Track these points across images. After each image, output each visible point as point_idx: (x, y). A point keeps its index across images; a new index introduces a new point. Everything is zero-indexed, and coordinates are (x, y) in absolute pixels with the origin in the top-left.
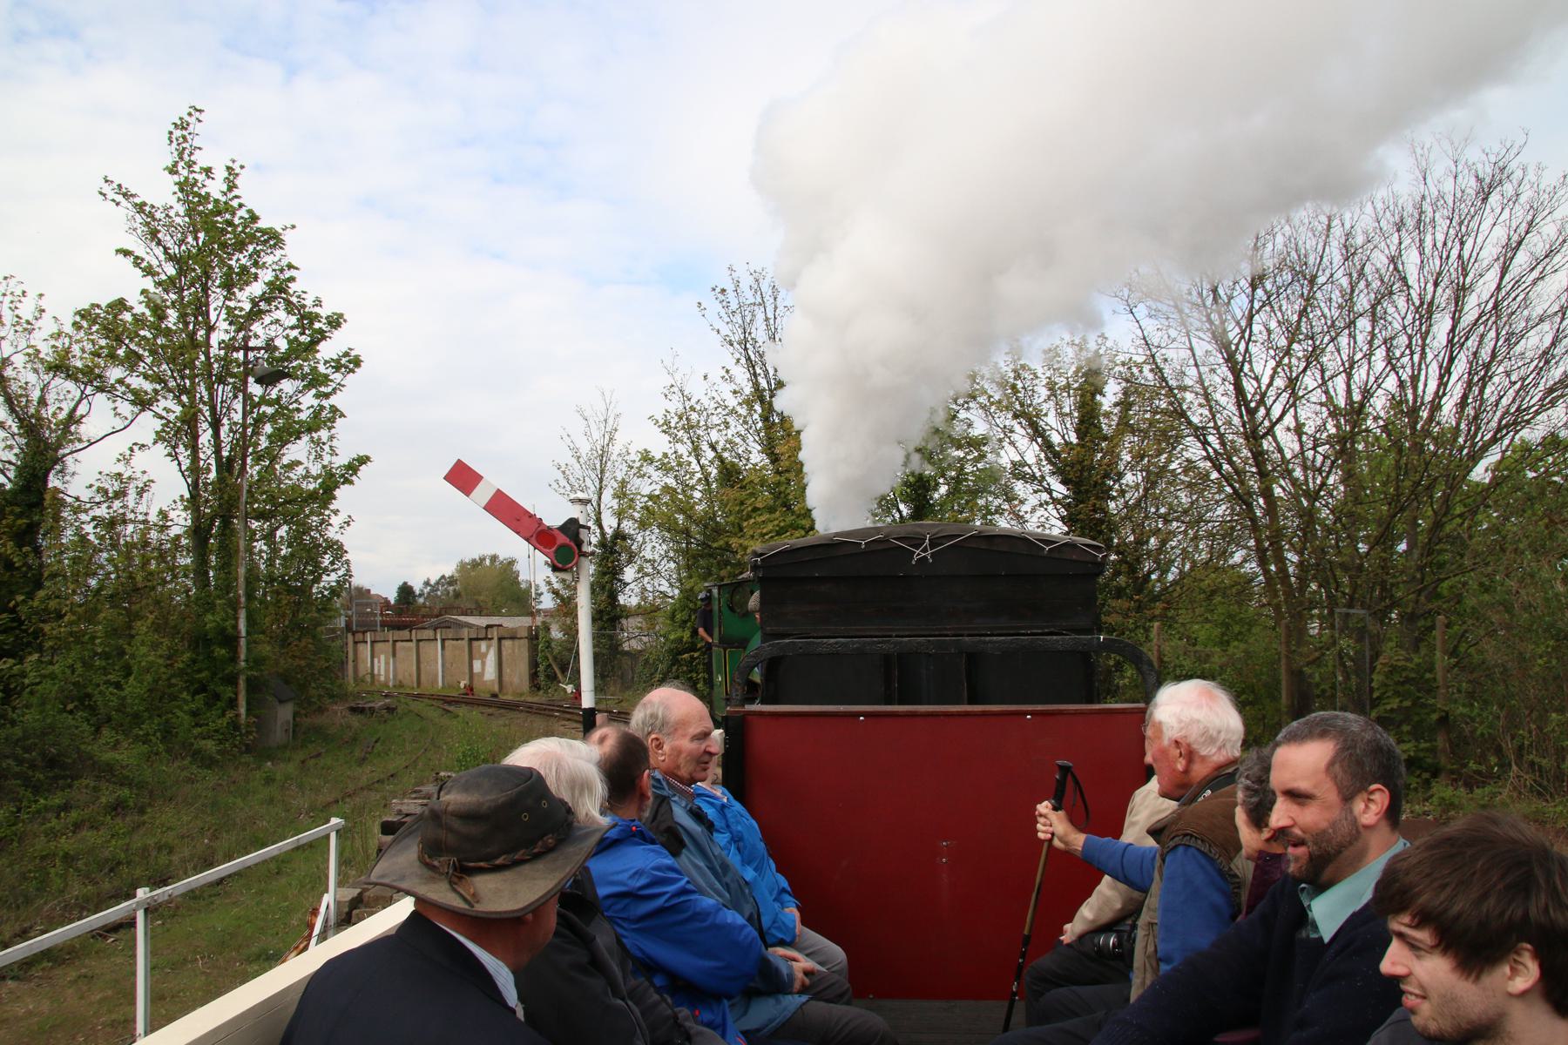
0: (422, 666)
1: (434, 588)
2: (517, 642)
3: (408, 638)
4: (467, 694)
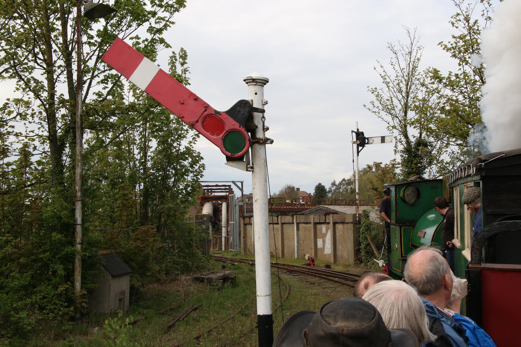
0: (285, 242)
1: (338, 187)
2: (346, 225)
3: (276, 222)
4: (309, 265)
